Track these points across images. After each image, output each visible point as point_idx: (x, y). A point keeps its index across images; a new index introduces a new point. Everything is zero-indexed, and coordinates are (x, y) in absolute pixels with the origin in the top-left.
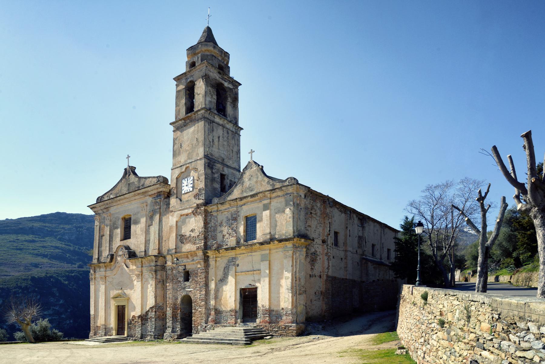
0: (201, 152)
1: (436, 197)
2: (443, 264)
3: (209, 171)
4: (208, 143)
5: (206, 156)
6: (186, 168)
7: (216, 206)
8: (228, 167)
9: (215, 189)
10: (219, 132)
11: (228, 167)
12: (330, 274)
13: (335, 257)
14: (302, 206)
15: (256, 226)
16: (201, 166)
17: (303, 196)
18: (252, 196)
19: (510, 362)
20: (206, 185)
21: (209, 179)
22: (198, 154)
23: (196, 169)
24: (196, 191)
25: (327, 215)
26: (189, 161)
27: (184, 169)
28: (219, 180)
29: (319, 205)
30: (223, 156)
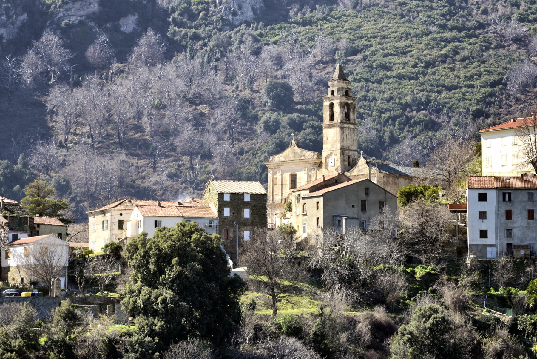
0: (338, 146)
1: (376, 133)
2: (235, 293)
3: (342, 156)
4: (342, 141)
5: (341, 149)
6: (331, 153)
7: (188, 158)
8: (351, 150)
9: (345, 165)
10: (347, 132)
11: (351, 150)
12: (527, 199)
13: (306, 217)
14: (382, 182)
15: (231, 180)
16: (338, 152)
17: (382, 177)
18: (362, 175)
19: (486, 218)
20: (341, 165)
21: (343, 161)
22: (337, 147)
23: (335, 155)
24: (336, 167)
25: (396, 183)
26: (332, 149)
27: (330, 152)
28: (347, 160)
29: (391, 179)
30: (349, 145)
